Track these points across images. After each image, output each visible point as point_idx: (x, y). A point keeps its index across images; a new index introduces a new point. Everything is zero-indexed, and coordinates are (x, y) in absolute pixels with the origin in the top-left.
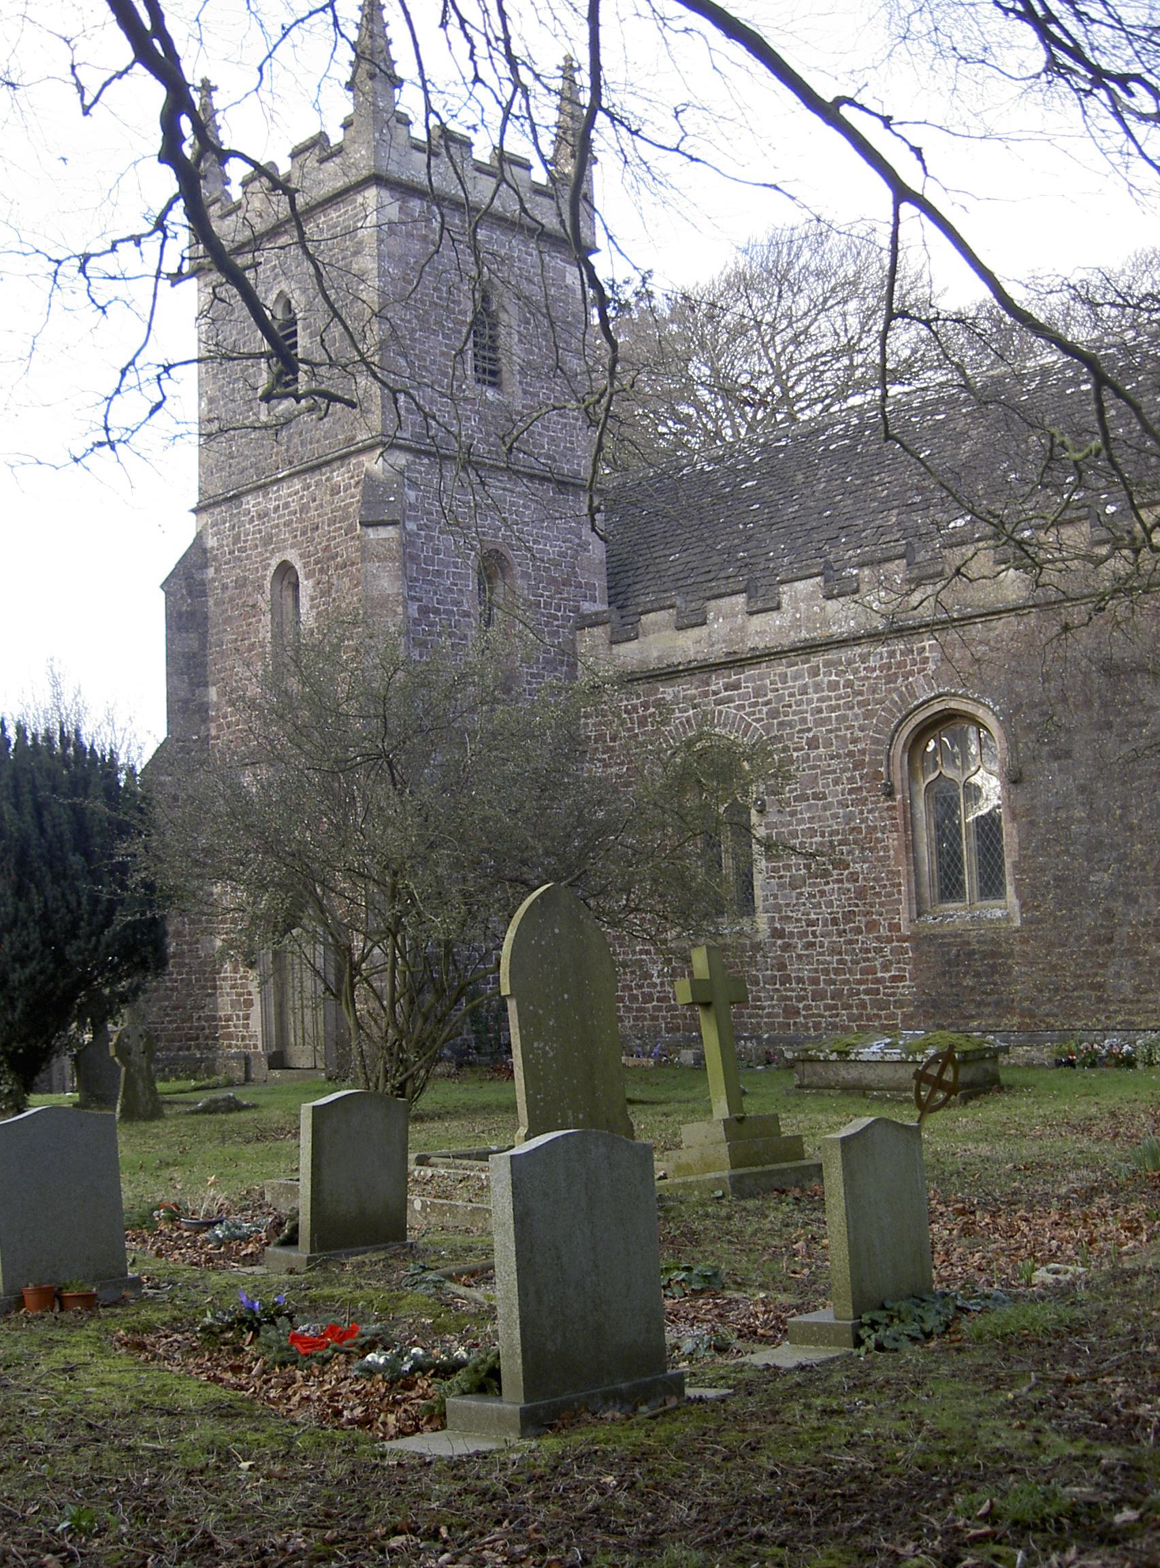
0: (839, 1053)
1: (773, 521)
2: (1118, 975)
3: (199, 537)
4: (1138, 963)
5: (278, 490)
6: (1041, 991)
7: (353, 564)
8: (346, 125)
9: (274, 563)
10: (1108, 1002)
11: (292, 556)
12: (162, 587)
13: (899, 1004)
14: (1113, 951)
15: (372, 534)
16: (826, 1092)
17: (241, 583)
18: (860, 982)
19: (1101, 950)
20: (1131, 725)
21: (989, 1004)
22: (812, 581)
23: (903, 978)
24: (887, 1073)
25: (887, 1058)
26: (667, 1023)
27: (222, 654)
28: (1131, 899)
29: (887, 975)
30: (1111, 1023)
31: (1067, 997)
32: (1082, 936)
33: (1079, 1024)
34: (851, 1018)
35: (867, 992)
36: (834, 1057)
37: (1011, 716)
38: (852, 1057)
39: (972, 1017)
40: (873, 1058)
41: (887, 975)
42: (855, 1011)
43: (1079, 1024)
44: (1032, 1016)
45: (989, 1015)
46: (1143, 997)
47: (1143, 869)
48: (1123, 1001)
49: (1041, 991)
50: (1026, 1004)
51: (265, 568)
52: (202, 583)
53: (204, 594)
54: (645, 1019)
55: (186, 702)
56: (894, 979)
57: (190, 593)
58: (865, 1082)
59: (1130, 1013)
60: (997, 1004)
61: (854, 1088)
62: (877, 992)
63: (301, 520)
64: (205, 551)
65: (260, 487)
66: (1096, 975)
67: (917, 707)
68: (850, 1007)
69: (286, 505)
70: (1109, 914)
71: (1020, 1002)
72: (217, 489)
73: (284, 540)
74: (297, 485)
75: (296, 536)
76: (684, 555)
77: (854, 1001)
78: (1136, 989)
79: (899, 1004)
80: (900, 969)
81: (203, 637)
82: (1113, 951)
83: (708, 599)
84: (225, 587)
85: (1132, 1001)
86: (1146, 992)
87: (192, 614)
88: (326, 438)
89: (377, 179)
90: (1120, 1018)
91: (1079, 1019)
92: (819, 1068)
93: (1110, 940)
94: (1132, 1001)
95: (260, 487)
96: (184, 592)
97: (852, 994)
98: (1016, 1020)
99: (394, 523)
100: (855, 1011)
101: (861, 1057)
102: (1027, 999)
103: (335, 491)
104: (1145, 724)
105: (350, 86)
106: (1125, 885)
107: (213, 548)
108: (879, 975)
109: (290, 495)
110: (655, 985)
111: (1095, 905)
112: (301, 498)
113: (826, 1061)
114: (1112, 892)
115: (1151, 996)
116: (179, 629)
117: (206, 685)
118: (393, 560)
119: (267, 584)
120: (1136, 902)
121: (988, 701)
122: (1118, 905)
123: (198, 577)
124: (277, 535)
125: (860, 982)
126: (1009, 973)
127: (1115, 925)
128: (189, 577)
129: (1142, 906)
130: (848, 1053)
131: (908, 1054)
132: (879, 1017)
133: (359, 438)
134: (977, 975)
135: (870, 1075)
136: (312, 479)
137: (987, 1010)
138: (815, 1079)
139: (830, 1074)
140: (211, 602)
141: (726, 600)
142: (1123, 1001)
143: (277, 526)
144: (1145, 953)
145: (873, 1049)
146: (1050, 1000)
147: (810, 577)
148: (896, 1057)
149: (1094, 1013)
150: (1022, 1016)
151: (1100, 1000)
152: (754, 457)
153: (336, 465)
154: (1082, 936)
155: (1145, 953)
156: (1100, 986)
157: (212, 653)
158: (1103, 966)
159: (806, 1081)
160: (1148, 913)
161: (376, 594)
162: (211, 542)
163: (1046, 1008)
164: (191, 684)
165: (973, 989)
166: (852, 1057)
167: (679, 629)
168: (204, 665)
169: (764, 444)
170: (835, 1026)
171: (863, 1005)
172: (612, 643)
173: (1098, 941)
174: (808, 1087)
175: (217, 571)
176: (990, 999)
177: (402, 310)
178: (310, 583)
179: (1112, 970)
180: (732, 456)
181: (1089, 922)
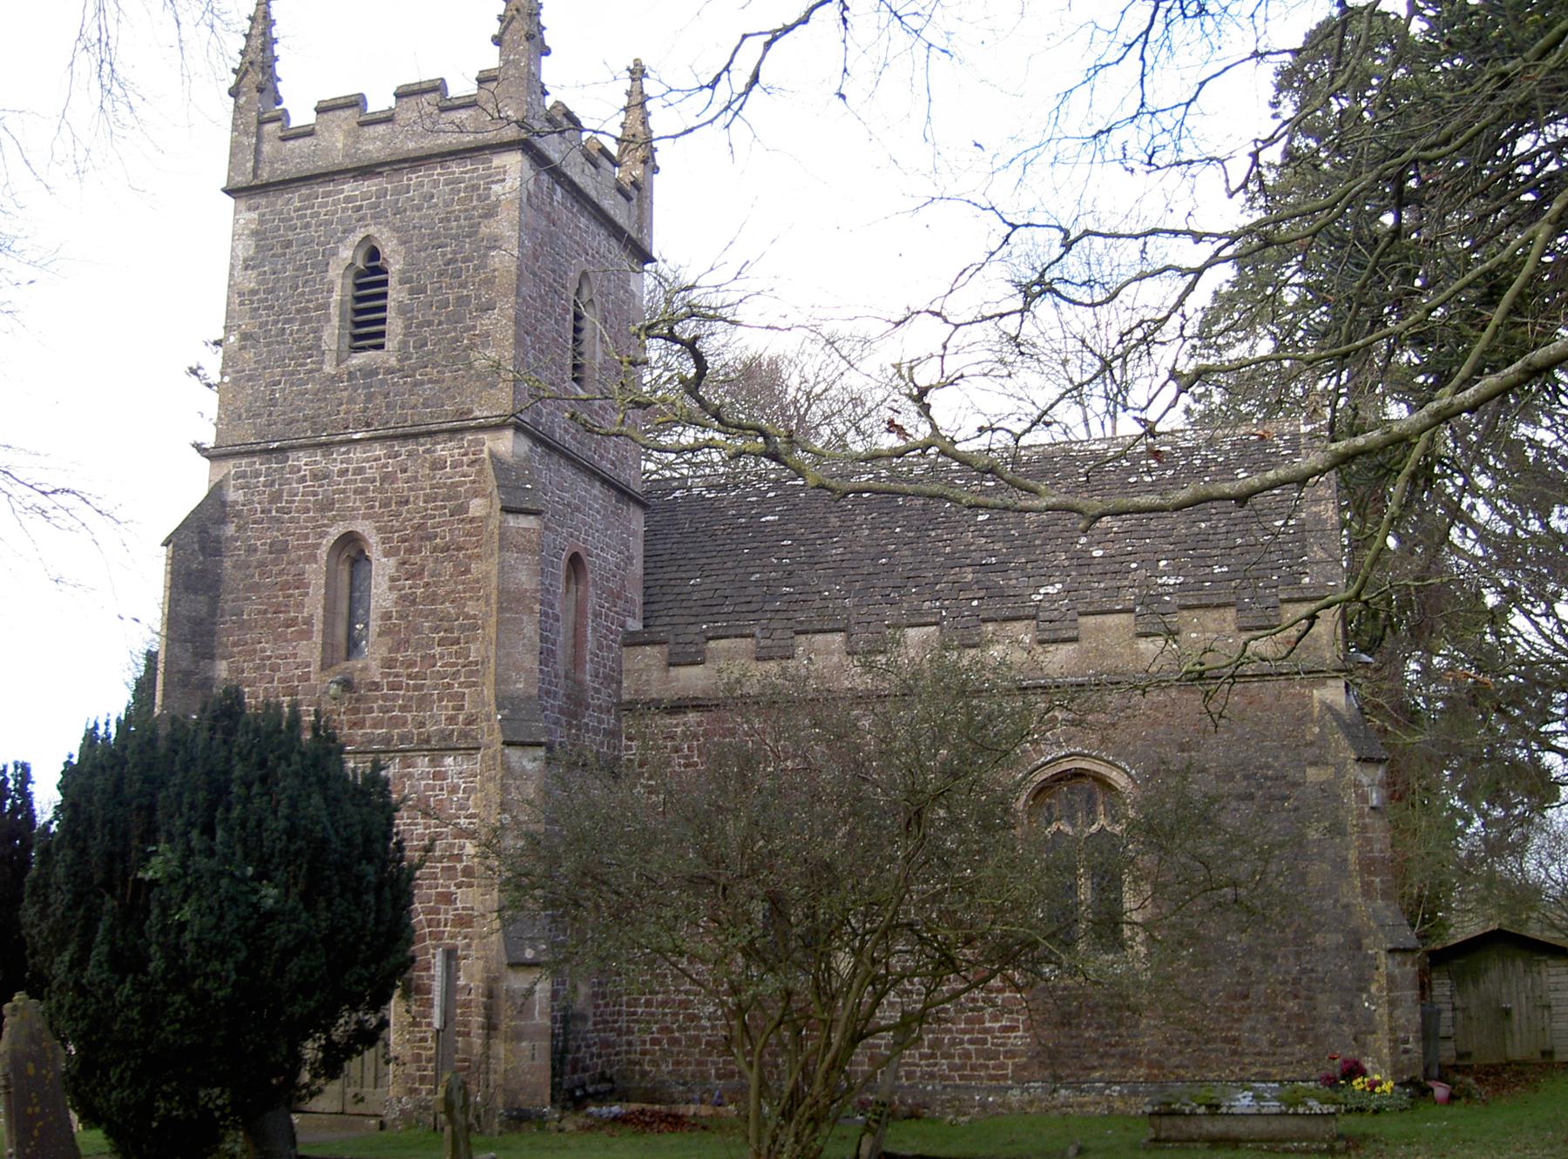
0: (1209, 1106)
1: (816, 560)
2: (1253, 1029)
3: (216, 491)
4: (1276, 1019)
5: (348, 452)
6: (1170, 1044)
7: (459, 549)
8: (483, 79)
9: (335, 532)
10: (1242, 1054)
11: (363, 527)
12: (166, 544)
13: (1010, 1054)
14: (1249, 1008)
15: (513, 521)
16: (1191, 1145)
17: (278, 549)
18: (964, 1032)
19: (1236, 1005)
20: (1272, 798)
21: (1113, 1056)
22: (926, 629)
23: (1014, 1029)
24: (1259, 1126)
25: (1264, 1111)
26: (717, 1070)
27: (242, 625)
28: (1268, 958)
29: (997, 1025)
30: (1245, 1075)
31: (1200, 1050)
32: (1217, 992)
33: (1211, 1076)
34: (952, 1068)
35: (971, 1042)
36: (1202, 1110)
37: (1148, 780)
38: (1224, 1110)
39: (1094, 1068)
40: (1249, 1111)
41: (997, 1025)
42: (957, 1060)
43: (1211, 1076)
44: (1161, 1067)
45: (1114, 1067)
46: (1279, 1050)
47: (1282, 931)
48: (1259, 1054)
49: (1170, 1044)
50: (1155, 1056)
51: (322, 535)
52: (218, 540)
53: (218, 552)
54: (689, 1063)
55: (188, 674)
56: (1005, 1029)
57: (203, 549)
58: (1233, 1135)
59: (1266, 1065)
60: (1123, 1055)
61: (1221, 1139)
62: (985, 1041)
63: (381, 490)
64: (224, 504)
65: (321, 445)
66: (1231, 1029)
67: (1044, 764)
68: (952, 1056)
69: (360, 471)
70: (1245, 971)
71: (1149, 1053)
72: (246, 434)
73: (358, 509)
74: (379, 450)
75: (372, 507)
76: (708, 580)
77: (958, 1049)
78: (1272, 1043)
79: (1010, 1054)
80: (1012, 1020)
81: (215, 600)
82: (1249, 1008)
83: (798, 633)
84: (252, 550)
85: (1267, 1055)
86: (1282, 1046)
87: (203, 573)
88: (425, 405)
89: (526, 147)
90: (1255, 1070)
91: (1211, 1071)
92: (1179, 1121)
93: (1247, 997)
94: (1267, 1055)
95: (321, 445)
96: (196, 547)
97: (953, 1043)
98: (1143, 1071)
99: (537, 513)
100: (957, 1060)
101: (1234, 1110)
102: (1155, 1051)
103: (438, 465)
104: (1287, 798)
105: (497, 40)
106: (1263, 945)
107: (236, 502)
108: (988, 1025)
109: (367, 460)
110: (704, 1028)
111: (1233, 963)
112: (385, 466)
113: (1193, 1114)
114: (1249, 952)
115: (1287, 1049)
116: (187, 589)
117: (212, 657)
118: (533, 553)
119: (322, 553)
120: (1275, 961)
121: (1123, 764)
122: (1256, 965)
123: (213, 532)
124: (342, 501)
125: (964, 1032)
126: (1136, 1026)
127: (1252, 983)
128: (203, 530)
129: (1279, 966)
130: (1218, 1107)
131: (1289, 1106)
132: (987, 1067)
133: (477, 413)
134: (1101, 1027)
135: (1238, 1128)
136: (403, 449)
137: (1111, 1062)
138: (1173, 1133)
139: (1192, 1128)
140: (228, 563)
141: (819, 637)
142: (1259, 1054)
143: (344, 491)
144: (1283, 1009)
145: (1243, 1101)
146: (1180, 1052)
147: (925, 625)
148: (1274, 1110)
149: (1228, 1065)
150: (1150, 1066)
151: (1234, 1053)
152: (767, 492)
153: (441, 437)
154: (1217, 992)
155: (1283, 1009)
156: (1235, 1040)
157: (225, 623)
158: (1239, 1020)
159: (1163, 1135)
160: (1287, 972)
161: (513, 587)
162: (233, 495)
163: (1175, 1061)
164: (196, 654)
165: (1095, 1040)
166: (1224, 1110)
167: (758, 659)
168: (211, 633)
169: (776, 481)
170: (932, 1076)
171: (967, 1055)
172: (671, 665)
173: (1234, 997)
174: (1167, 1140)
175: (239, 528)
176: (1113, 1051)
177: (448, 276)
178: (392, 561)
179: (1248, 1024)
180: (736, 486)
181: (1226, 979)
